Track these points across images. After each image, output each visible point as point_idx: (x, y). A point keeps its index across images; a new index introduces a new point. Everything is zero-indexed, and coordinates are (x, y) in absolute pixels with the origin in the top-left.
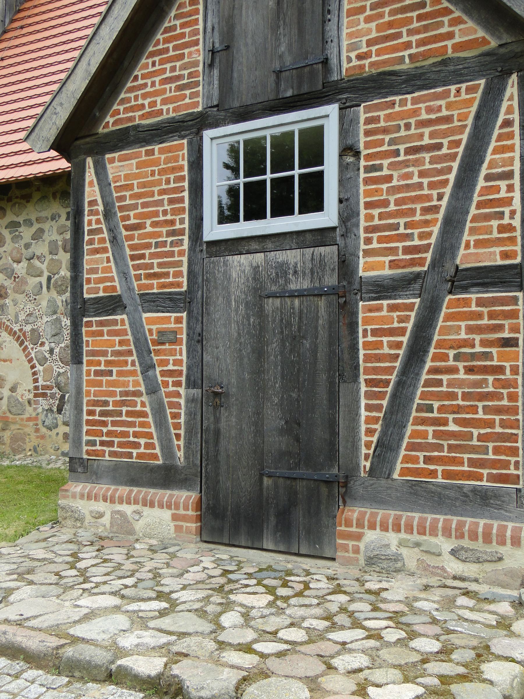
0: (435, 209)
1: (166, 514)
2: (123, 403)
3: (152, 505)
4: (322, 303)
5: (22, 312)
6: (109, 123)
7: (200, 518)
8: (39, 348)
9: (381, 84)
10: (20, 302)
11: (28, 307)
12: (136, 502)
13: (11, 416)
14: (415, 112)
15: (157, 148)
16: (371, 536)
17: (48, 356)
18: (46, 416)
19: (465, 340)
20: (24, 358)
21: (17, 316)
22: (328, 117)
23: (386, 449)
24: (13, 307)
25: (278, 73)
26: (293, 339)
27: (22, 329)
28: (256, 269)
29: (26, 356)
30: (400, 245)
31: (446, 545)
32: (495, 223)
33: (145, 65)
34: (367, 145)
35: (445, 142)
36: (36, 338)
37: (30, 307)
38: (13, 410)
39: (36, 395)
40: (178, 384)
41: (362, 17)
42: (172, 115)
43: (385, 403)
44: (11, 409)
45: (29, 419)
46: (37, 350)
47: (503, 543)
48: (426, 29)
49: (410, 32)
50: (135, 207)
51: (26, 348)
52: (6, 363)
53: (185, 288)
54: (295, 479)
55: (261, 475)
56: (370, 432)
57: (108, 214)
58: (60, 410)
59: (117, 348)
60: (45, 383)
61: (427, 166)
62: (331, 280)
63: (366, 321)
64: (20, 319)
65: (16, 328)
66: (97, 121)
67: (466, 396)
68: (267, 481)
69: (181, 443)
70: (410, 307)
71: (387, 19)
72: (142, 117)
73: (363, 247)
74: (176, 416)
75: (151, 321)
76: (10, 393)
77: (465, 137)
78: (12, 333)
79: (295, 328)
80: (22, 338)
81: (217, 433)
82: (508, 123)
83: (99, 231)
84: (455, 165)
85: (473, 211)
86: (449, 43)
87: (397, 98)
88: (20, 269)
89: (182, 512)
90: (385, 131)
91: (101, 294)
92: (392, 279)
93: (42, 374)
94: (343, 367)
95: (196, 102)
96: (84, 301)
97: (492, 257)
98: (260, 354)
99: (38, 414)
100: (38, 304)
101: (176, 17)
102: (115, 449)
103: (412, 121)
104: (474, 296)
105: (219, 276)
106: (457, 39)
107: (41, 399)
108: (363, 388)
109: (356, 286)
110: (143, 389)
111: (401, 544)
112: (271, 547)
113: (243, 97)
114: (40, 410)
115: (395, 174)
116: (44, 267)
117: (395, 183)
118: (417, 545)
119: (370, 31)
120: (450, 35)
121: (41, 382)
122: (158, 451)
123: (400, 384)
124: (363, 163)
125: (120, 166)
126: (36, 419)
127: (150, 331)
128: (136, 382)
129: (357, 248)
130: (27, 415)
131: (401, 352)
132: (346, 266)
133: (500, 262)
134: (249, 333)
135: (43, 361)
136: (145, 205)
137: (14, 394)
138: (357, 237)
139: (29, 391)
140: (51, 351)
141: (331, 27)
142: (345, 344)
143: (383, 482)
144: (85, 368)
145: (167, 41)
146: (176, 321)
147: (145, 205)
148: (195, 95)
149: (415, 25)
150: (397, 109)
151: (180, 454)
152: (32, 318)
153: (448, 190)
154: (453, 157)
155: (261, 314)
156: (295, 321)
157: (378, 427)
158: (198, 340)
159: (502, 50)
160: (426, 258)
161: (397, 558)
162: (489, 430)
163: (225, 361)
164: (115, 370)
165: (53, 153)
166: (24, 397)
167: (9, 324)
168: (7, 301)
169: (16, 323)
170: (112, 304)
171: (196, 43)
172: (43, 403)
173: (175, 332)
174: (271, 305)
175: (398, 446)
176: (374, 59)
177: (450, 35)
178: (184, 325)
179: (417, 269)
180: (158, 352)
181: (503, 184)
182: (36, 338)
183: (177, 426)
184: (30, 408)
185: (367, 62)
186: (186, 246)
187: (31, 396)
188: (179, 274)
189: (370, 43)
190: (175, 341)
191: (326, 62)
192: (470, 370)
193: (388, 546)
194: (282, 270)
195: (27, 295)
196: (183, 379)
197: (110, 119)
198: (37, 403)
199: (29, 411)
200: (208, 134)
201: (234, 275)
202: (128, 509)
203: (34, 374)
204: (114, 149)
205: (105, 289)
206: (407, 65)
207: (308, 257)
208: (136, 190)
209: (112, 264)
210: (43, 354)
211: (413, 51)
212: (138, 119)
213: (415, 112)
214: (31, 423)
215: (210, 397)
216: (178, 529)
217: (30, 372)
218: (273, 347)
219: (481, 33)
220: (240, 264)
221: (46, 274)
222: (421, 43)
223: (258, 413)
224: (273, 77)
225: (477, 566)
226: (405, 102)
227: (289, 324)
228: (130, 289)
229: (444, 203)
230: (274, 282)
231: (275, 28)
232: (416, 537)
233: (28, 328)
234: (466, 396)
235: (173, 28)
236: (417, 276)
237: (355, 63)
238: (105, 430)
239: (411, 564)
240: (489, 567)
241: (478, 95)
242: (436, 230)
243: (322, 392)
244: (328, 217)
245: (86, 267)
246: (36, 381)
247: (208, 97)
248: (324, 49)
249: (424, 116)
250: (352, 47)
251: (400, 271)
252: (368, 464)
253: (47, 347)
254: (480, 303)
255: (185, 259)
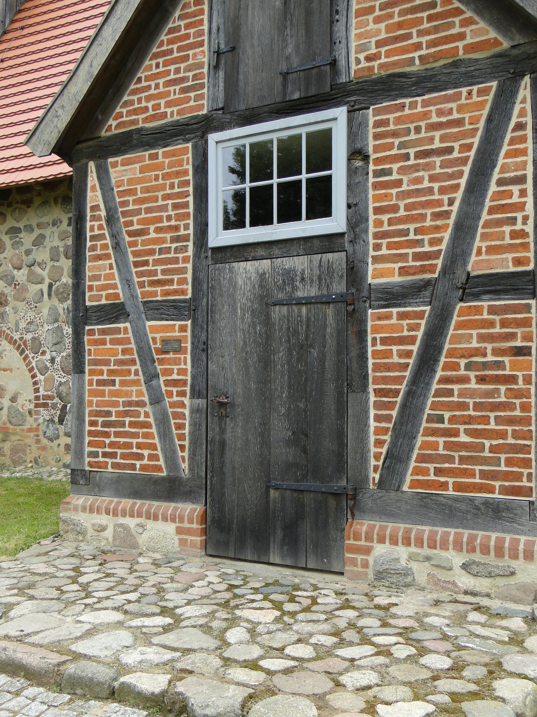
0: (446, 214)
1: (171, 528)
2: (126, 414)
3: (156, 518)
4: (330, 311)
5: (23, 320)
6: (112, 126)
7: (205, 532)
8: (40, 357)
9: (390, 86)
10: (20, 309)
11: (29, 315)
12: (139, 515)
13: (11, 427)
14: (426, 115)
15: (160, 151)
16: (380, 550)
17: (49, 365)
18: (48, 426)
19: (477, 349)
20: (25, 367)
21: (17, 325)
22: (336, 120)
23: (395, 461)
24: (14, 315)
25: (285, 75)
26: (300, 348)
27: (22, 338)
28: (262, 276)
29: (27, 365)
30: (410, 251)
31: (457, 559)
32: (507, 229)
33: (149, 67)
34: (377, 149)
35: (456, 145)
36: (37, 346)
37: (31, 315)
38: (14, 420)
39: (37, 406)
40: (182, 394)
41: (371, 18)
42: (176, 118)
43: (394, 413)
44: (12, 420)
45: (30, 430)
46: (38, 359)
47: (515, 557)
48: (436, 29)
49: (420, 33)
50: (138, 212)
51: (27, 357)
52: (6, 373)
53: (189, 296)
54: (302, 491)
55: (268, 487)
56: (379, 443)
57: (111, 219)
58: (61, 421)
59: (120, 357)
60: (46, 393)
61: (438, 170)
62: (339, 287)
63: (375, 329)
64: (21, 328)
65: (16, 336)
66: (100, 124)
67: (477, 406)
68: (273, 494)
69: (186, 454)
70: (420, 315)
71: (396, 19)
72: (145, 120)
73: (372, 253)
74: (180, 427)
75: (154, 330)
76: (10, 403)
77: (476, 141)
78: (12, 341)
79: (302, 337)
80: (23, 346)
81: (223, 444)
82: (520, 126)
83: (101, 237)
84: (467, 169)
85: (485, 216)
86: (460, 44)
87: (407, 101)
88: (21, 275)
89: (186, 525)
90: (395, 134)
91: (104, 302)
92: (402, 286)
93: (43, 383)
94: (352, 377)
95: (201, 104)
96: (87, 309)
97: (504, 263)
98: (266, 363)
99: (39, 425)
100: (39, 311)
101: (181, 18)
102: (118, 460)
103: (423, 124)
104: (485, 304)
105: (225, 283)
106: (469, 40)
107: (42, 409)
108: (372, 398)
109: (365, 293)
110: (146, 399)
111: (411, 558)
112: (277, 562)
113: (249, 99)
114: (41, 421)
115: (405, 179)
116: (45, 274)
117: (405, 187)
118: (428, 559)
119: (379, 31)
120: (461, 36)
121: (42, 392)
122: (161, 462)
123: (410, 394)
124: (372, 167)
125: (123, 170)
126: (37, 429)
127: (154, 339)
128: (139, 392)
129: (366, 254)
130: (27, 426)
131: (411, 361)
132: (354, 272)
133: (512, 269)
134: (255, 341)
135: (44, 370)
136: (148, 210)
137: (14, 404)
138: (366, 243)
139: (30, 401)
140: (53, 360)
141: (339, 28)
142: (354, 353)
143: (393, 494)
144: (87, 377)
145: (171, 42)
146: (181, 329)
147: (148, 210)
148: (200, 97)
149: (426, 25)
150: (407, 111)
151: (185, 466)
152: (32, 326)
153: (459, 195)
154: (464, 161)
155: (267, 322)
156: (302, 329)
157: (387, 438)
158: (202, 349)
159: (515, 52)
160: (436, 265)
161: (407, 572)
162: (501, 441)
163: (231, 370)
164: (117, 379)
165: (55, 157)
166: (24, 408)
167: (9, 332)
168: (7, 309)
169: (16, 332)
170: (115, 312)
171: (201, 44)
172: (44, 414)
173: (179, 341)
174: (278, 313)
175: (408, 458)
176: (383, 60)
177: (461, 36)
178: (189, 333)
179: (428, 276)
180: (162, 361)
181: (515, 189)
182: (37, 346)
183: (181, 437)
184: (30, 419)
185: (376, 64)
186: (190, 252)
187: (32, 406)
188: (183, 281)
189: (379, 44)
190: (180, 350)
191: (334, 63)
192: (481, 380)
193: (397, 560)
194: (289, 276)
195: (27, 303)
196: (188, 389)
197: (113, 123)
198: (38, 413)
199: (30, 422)
200: (213, 138)
201: (240, 282)
202: (131, 522)
203: (35, 383)
204: (116, 153)
205: (108, 297)
206: (417, 66)
207: (316, 263)
208: (139, 195)
209: (115, 271)
210: (44, 363)
211: (424, 52)
212: (141, 122)
213: (426, 115)
214: (32, 434)
215: (215, 407)
216: (182, 542)
217: (31, 381)
218: (280, 356)
219: (493, 34)
220: (246, 271)
221: (47, 281)
222: (431, 44)
223: (265, 424)
224: (280, 79)
225: (489, 580)
226: (415, 105)
227: (296, 333)
228: (133, 297)
229: (455, 208)
230: (281, 289)
231: (282, 29)
232: (426, 551)
233: (29, 337)
234: (477, 406)
235: (177, 29)
236: (428, 283)
237: (364, 64)
238: (107, 441)
239: (421, 578)
240: (501, 582)
241: (490, 97)
242: (447, 236)
243: (330, 402)
244: (336, 223)
245: (88, 273)
246: (37, 390)
247: (214, 99)
248: (332, 50)
249: (435, 119)
250: (361, 49)
251: (410, 278)
252: (377, 476)
253: (48, 356)
254: (492, 310)
255: (190, 266)
